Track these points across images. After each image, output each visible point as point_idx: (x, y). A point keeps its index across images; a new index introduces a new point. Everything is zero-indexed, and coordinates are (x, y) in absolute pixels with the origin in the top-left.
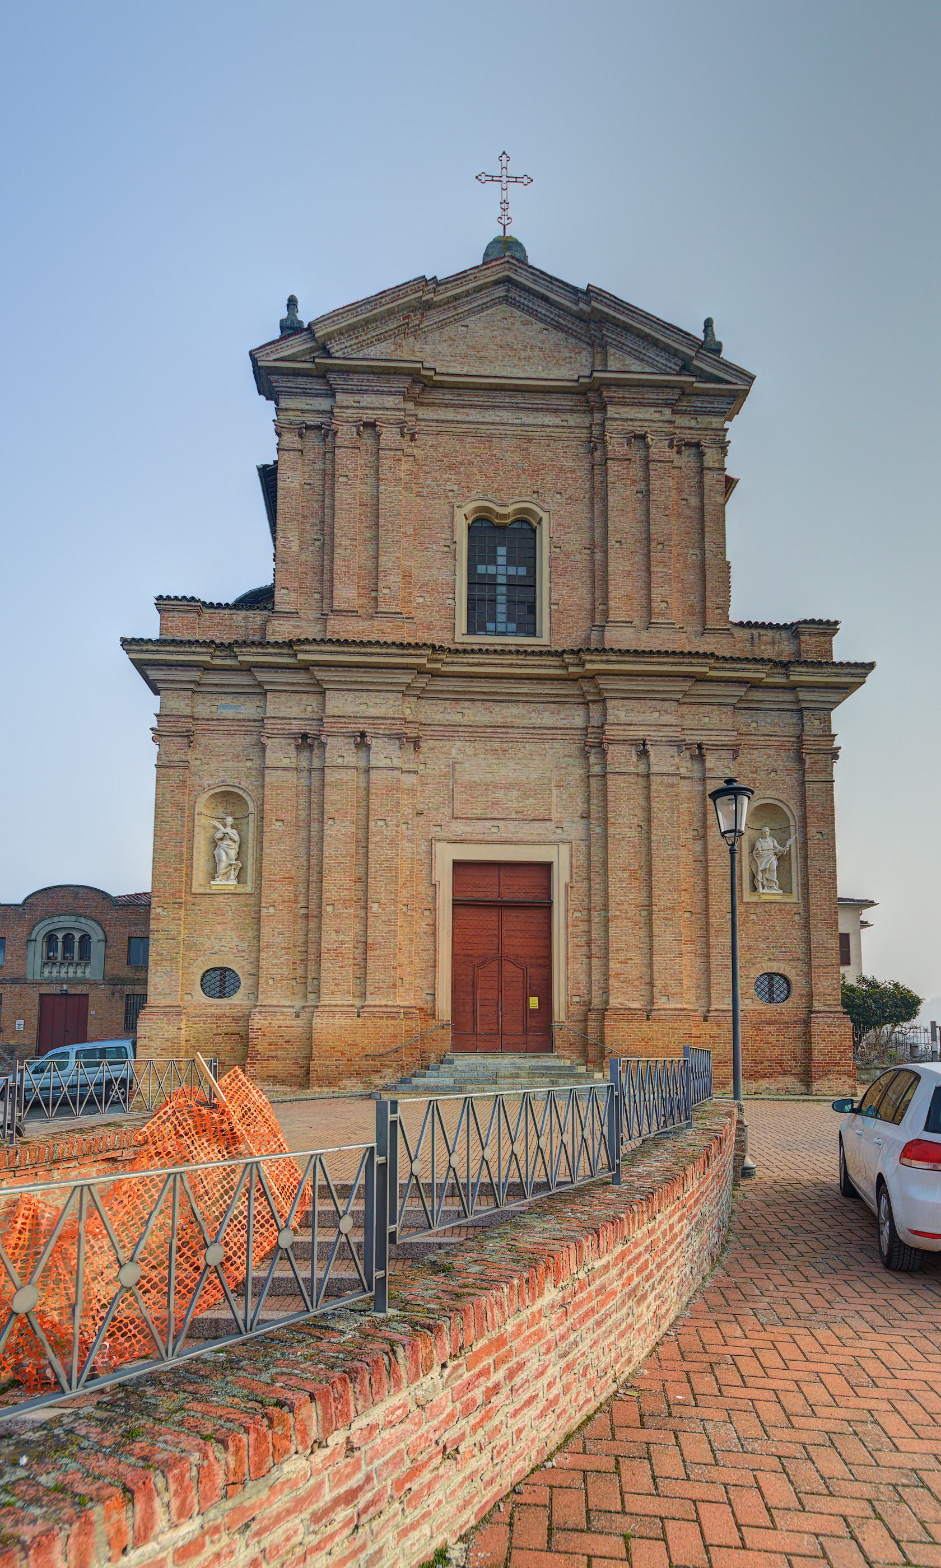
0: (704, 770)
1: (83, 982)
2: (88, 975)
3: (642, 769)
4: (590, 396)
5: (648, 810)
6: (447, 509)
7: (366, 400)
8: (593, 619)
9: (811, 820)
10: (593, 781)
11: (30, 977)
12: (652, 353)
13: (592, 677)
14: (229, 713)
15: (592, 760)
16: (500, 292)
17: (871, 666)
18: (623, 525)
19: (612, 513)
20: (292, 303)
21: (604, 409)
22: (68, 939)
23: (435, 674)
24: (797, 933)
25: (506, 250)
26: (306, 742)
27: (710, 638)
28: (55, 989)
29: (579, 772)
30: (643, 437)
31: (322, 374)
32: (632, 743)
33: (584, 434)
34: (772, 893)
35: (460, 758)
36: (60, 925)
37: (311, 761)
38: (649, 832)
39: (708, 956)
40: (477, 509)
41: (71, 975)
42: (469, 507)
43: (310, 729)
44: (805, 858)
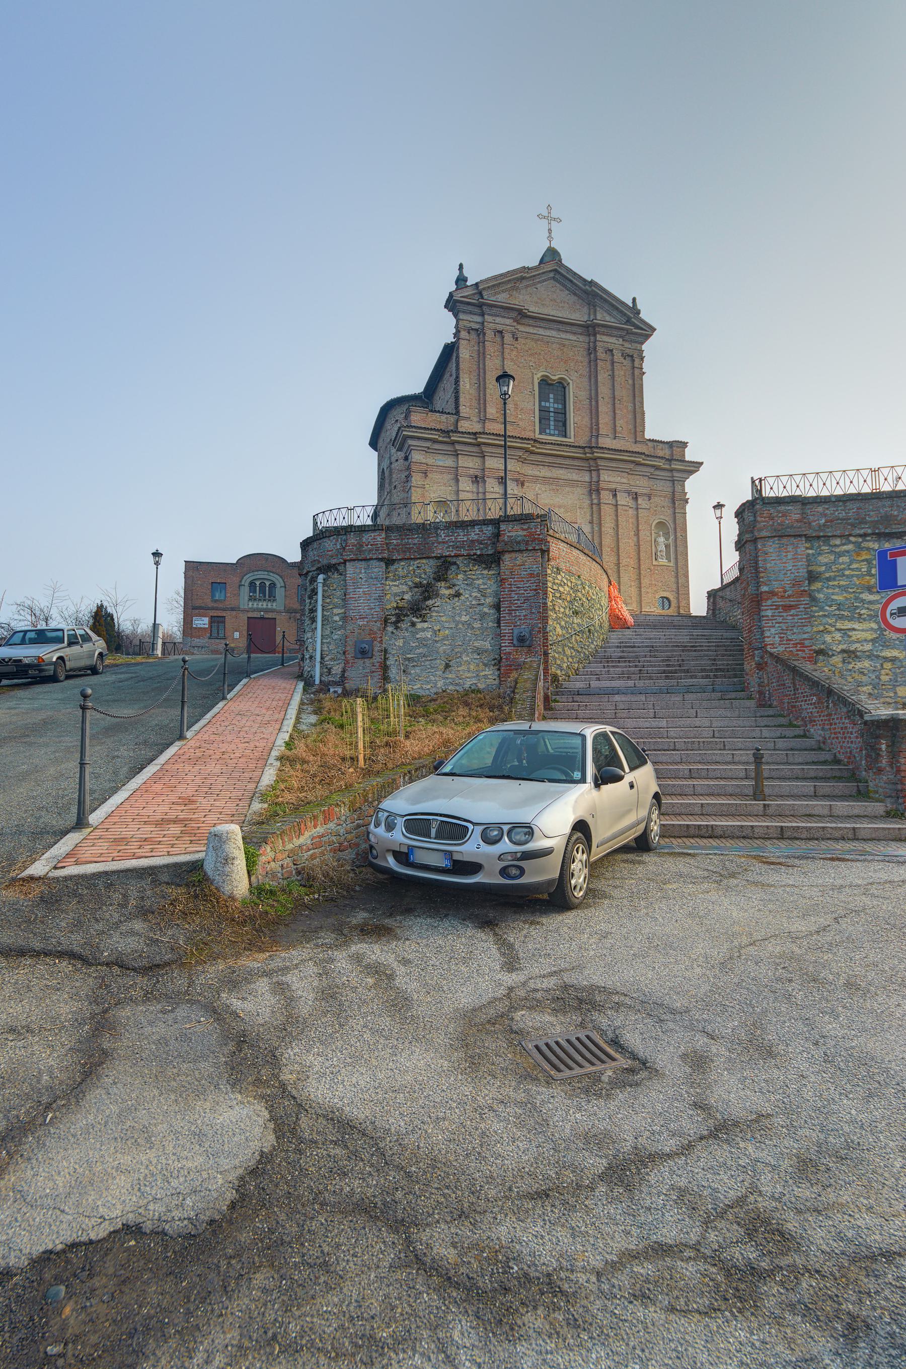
0: (637, 505)
1: (272, 611)
2: (274, 607)
3: (614, 502)
4: (590, 329)
5: (617, 521)
6: (530, 374)
7: (498, 320)
8: (592, 432)
9: (678, 530)
10: (594, 506)
11: (242, 607)
12: (615, 313)
13: (595, 459)
14: (441, 463)
15: (594, 497)
16: (552, 275)
17: (702, 463)
18: (604, 390)
19: (599, 384)
20: (461, 266)
21: (595, 335)
22: (263, 585)
23: (532, 453)
24: (673, 580)
25: (552, 254)
26: (477, 479)
27: (638, 445)
28: (256, 614)
29: (587, 502)
30: (611, 351)
31: (480, 306)
32: (610, 490)
33: (586, 346)
34: (663, 561)
35: (539, 492)
36: (258, 577)
37: (478, 489)
38: (617, 531)
39: (640, 588)
40: (543, 376)
41: (265, 606)
42: (540, 375)
43: (479, 474)
44: (676, 547)
